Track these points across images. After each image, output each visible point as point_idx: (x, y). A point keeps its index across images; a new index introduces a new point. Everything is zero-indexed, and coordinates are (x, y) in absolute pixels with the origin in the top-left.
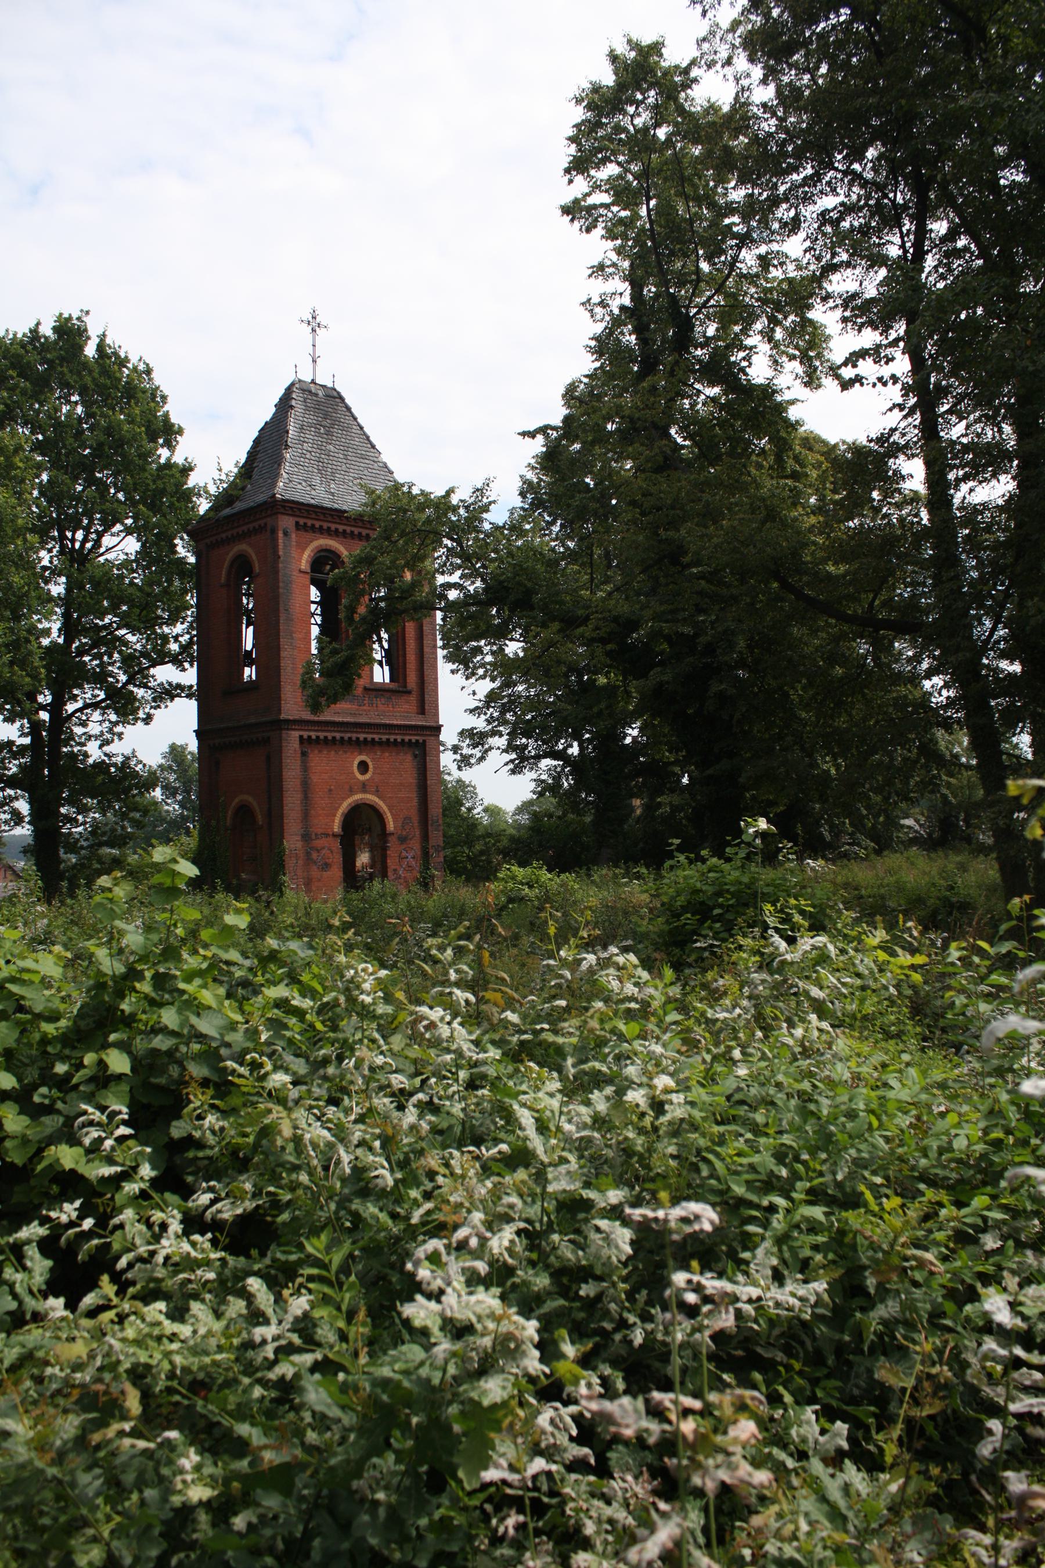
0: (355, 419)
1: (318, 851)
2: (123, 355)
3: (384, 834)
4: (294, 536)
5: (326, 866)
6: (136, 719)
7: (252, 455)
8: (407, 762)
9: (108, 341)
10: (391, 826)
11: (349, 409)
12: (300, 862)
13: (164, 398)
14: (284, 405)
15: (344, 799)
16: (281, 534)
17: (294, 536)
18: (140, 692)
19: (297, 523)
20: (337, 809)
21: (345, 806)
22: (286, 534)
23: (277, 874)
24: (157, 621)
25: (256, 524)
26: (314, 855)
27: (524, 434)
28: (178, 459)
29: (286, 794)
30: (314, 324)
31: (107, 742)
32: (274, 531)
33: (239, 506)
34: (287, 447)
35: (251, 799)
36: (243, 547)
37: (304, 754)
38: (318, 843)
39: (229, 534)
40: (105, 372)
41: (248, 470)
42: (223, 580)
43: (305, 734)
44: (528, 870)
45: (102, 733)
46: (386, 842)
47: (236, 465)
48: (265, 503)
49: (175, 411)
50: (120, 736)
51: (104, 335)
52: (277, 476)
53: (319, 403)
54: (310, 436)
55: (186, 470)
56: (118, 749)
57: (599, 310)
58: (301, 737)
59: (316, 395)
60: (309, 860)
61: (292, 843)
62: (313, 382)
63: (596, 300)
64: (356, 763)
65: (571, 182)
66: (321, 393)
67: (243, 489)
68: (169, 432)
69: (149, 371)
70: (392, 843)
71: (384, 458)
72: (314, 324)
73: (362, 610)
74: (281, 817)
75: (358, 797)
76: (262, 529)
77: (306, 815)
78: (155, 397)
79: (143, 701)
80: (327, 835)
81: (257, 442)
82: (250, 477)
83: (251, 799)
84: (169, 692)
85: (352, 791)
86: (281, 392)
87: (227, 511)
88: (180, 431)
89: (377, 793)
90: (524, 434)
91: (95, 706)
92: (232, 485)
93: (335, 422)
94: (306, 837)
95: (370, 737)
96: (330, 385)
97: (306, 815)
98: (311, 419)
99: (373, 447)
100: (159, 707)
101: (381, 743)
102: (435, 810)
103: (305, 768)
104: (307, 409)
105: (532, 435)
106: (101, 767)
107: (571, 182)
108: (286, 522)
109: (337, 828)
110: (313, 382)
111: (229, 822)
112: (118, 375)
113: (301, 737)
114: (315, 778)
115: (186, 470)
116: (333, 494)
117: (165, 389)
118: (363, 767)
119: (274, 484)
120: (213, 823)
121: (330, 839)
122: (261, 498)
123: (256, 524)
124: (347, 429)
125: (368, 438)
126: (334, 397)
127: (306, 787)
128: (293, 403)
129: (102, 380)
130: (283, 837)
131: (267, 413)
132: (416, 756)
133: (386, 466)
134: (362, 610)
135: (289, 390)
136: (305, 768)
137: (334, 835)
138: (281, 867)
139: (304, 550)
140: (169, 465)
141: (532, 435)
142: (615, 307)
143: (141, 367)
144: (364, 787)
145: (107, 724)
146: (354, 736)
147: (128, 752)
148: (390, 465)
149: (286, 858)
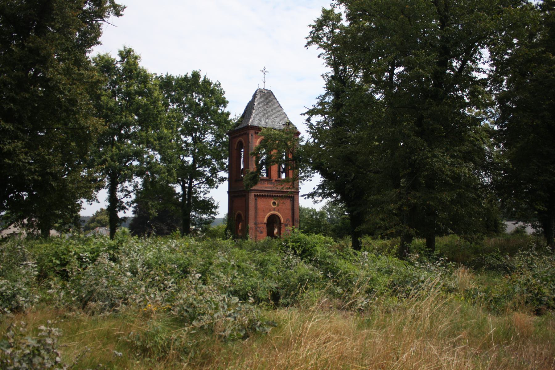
0: (276, 99)
1: (259, 228)
2: (210, 81)
3: (280, 224)
4: (254, 136)
5: (262, 232)
6: (214, 187)
7: (245, 111)
8: (288, 202)
9: (207, 78)
10: (282, 221)
11: (274, 96)
12: (253, 231)
13: (224, 92)
14: (255, 96)
15: (269, 212)
16: (250, 135)
17: (254, 136)
18: (215, 179)
19: (255, 132)
20: (266, 216)
21: (268, 215)
22: (252, 135)
23: (246, 234)
24: (222, 158)
25: (244, 132)
26: (258, 229)
27: (301, 114)
28: (226, 111)
29: (250, 211)
30: (264, 72)
31: (206, 194)
32: (248, 135)
33: (240, 127)
34: (254, 109)
35: (241, 212)
36: (240, 139)
37: (256, 199)
38: (260, 225)
39: (237, 135)
40: (205, 87)
41: (243, 116)
42: (236, 148)
43: (256, 194)
44: (318, 235)
45: (204, 191)
46: (281, 226)
47: (240, 115)
48: (246, 126)
49: (227, 96)
50: (209, 192)
51: (206, 76)
52: (250, 118)
53: (265, 95)
54: (261, 105)
55: (228, 114)
56: (208, 196)
57: (325, 77)
58: (255, 195)
59: (264, 93)
60: (256, 230)
61: (251, 225)
62: (264, 89)
63: (324, 75)
64: (272, 202)
65: (307, 48)
66: (266, 92)
67: (241, 121)
68: (224, 103)
69: (220, 84)
70: (283, 226)
71: (284, 111)
72: (264, 72)
73: (260, 162)
74: (248, 218)
75: (272, 212)
76: (245, 134)
77: (256, 217)
78: (222, 92)
79: (216, 182)
80: (262, 223)
81: (247, 107)
82: (244, 118)
83: (241, 212)
84: (222, 180)
85: (270, 211)
86: (254, 92)
87: (237, 128)
88: (228, 102)
89: (278, 211)
90: (301, 114)
91: (203, 183)
92: (239, 121)
93: (270, 101)
94: (256, 224)
95: (276, 195)
96: (269, 89)
97: (256, 217)
98: (262, 100)
99: (281, 108)
100: (220, 184)
101: (280, 196)
102: (297, 217)
103: (256, 203)
104: (261, 97)
105: (304, 114)
106: (204, 201)
107: (307, 48)
108: (252, 132)
109: (265, 221)
110: (264, 89)
111: (235, 218)
112: (209, 88)
113: (255, 195)
114: (259, 207)
115: (228, 114)
116: (267, 123)
117: (224, 90)
118: (274, 203)
119: (249, 121)
120: (231, 219)
121: (263, 224)
122: (245, 125)
123: (244, 132)
124: (273, 102)
125: (280, 105)
126: (270, 93)
127: (256, 209)
128: (257, 96)
129: (204, 90)
130: (248, 224)
131: (250, 98)
132: (291, 201)
133: (285, 113)
134: (260, 162)
135: (256, 92)
136: (256, 203)
137: (265, 223)
138: (247, 232)
139: (258, 138)
140: (223, 113)
141: (304, 114)
142: (330, 75)
143: (218, 83)
144: (274, 209)
145: (206, 188)
146: (271, 194)
147: (210, 197)
148: (286, 113)
149: (249, 230)
